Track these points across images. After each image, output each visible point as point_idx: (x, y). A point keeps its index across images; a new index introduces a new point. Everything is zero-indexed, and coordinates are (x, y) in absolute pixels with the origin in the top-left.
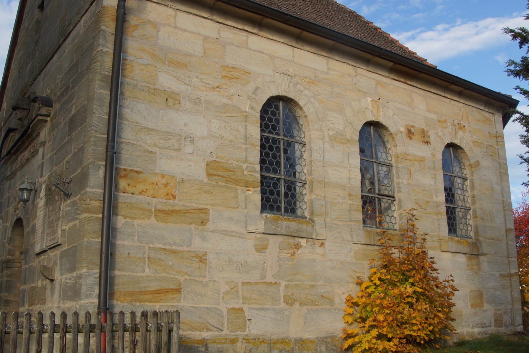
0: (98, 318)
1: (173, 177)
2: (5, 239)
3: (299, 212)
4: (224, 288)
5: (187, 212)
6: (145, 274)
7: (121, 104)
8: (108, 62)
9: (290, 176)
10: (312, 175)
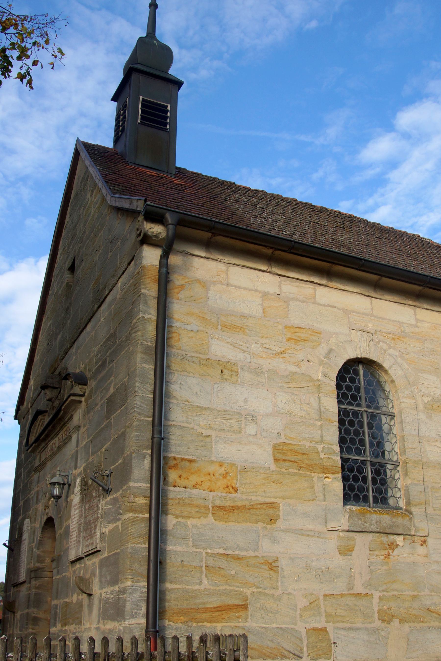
0: (147, 645)
1: (232, 465)
2: (33, 542)
3: (391, 502)
4: (302, 602)
5: (251, 507)
6: (202, 587)
7: (168, 380)
8: (151, 330)
9: (377, 456)
10: (405, 454)
